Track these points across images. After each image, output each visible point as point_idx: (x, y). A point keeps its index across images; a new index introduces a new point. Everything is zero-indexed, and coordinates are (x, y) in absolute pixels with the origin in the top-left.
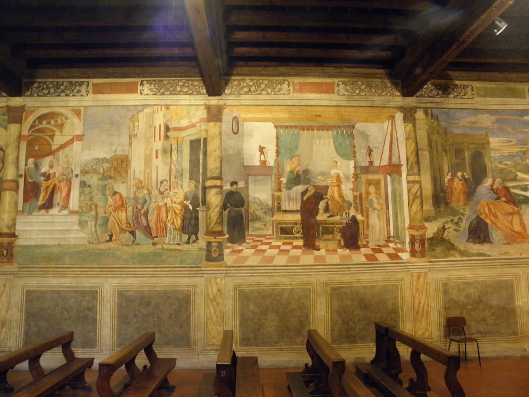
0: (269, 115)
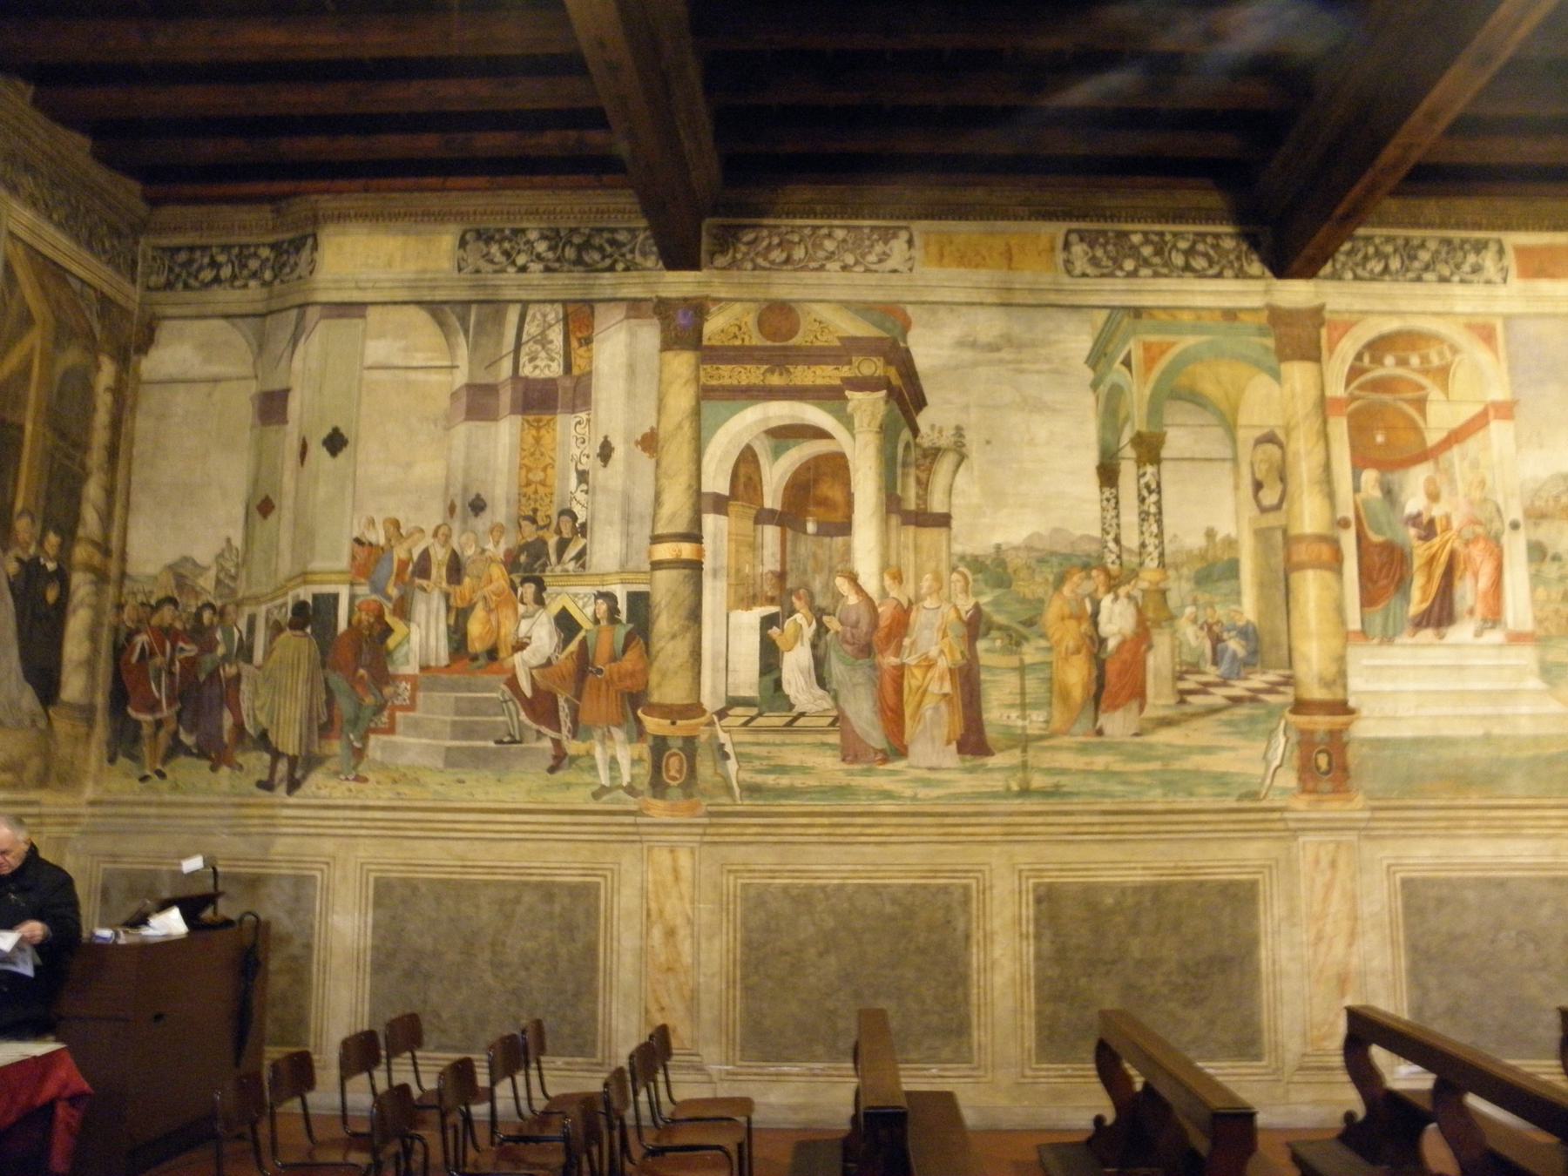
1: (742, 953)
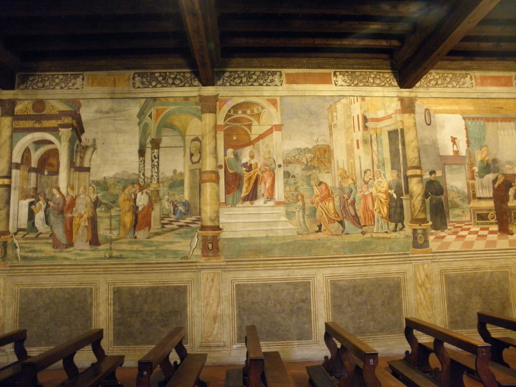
0: (456, 108)
1: (19, 312)
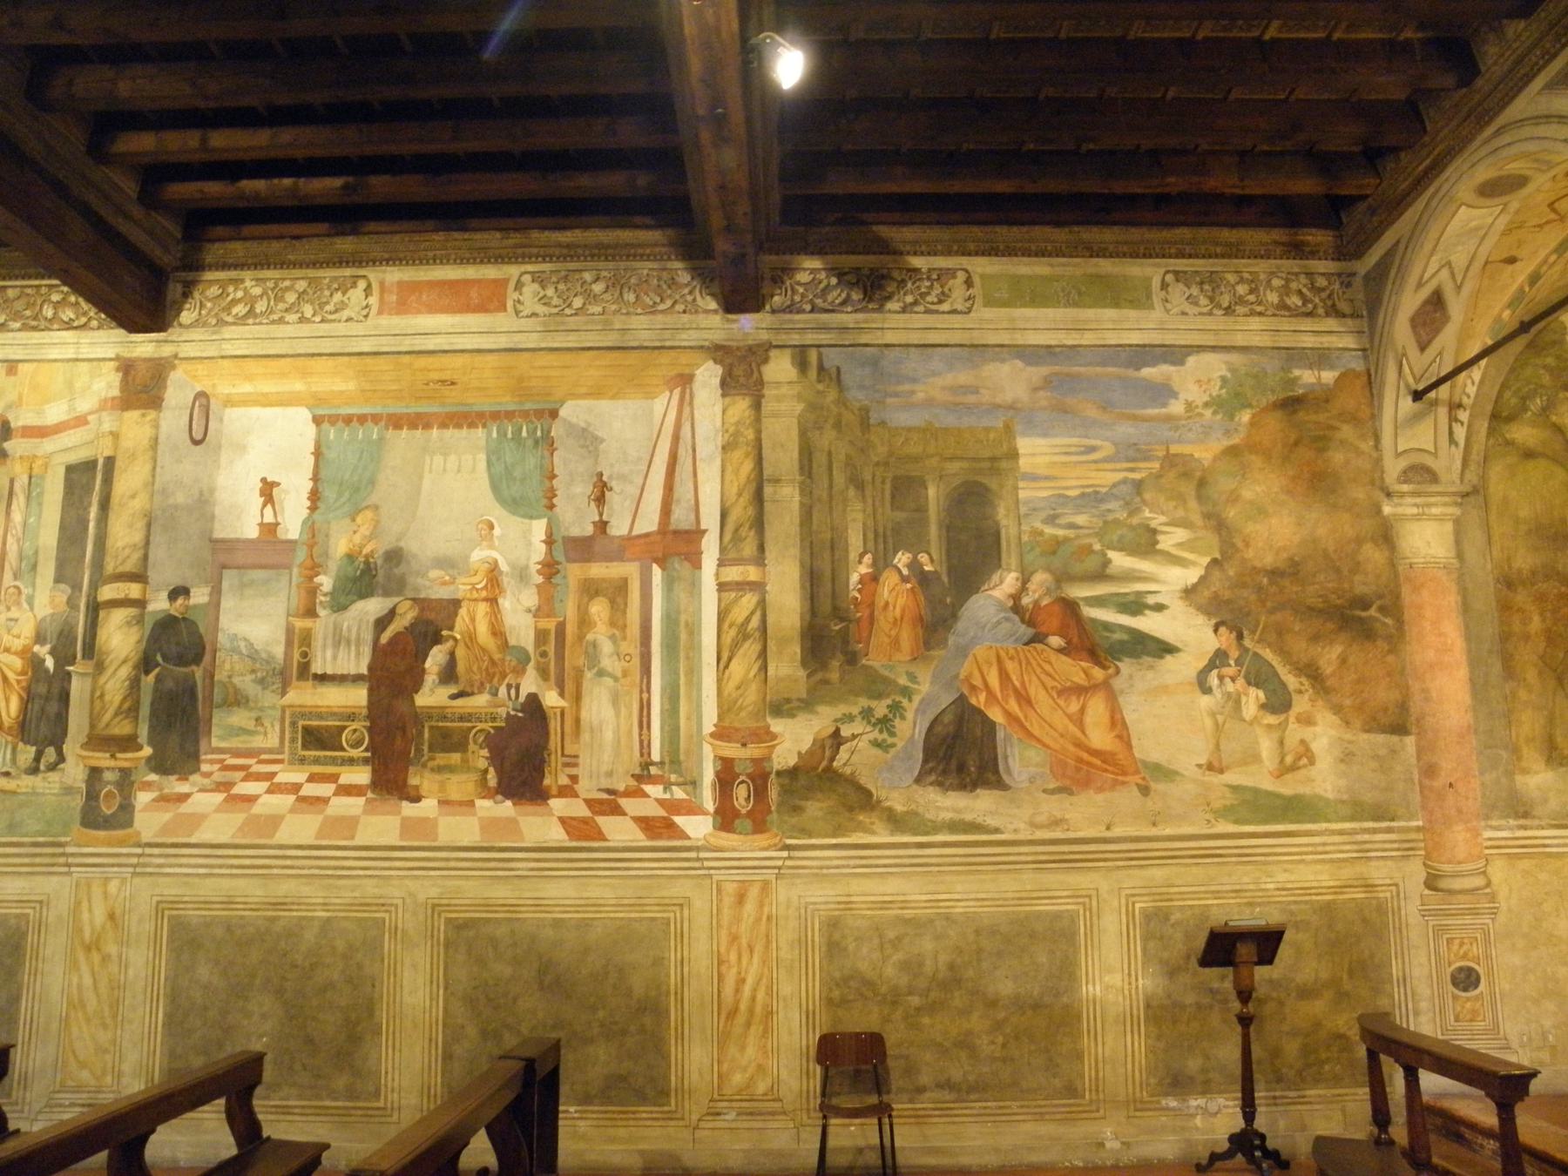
0: (298, 386)
